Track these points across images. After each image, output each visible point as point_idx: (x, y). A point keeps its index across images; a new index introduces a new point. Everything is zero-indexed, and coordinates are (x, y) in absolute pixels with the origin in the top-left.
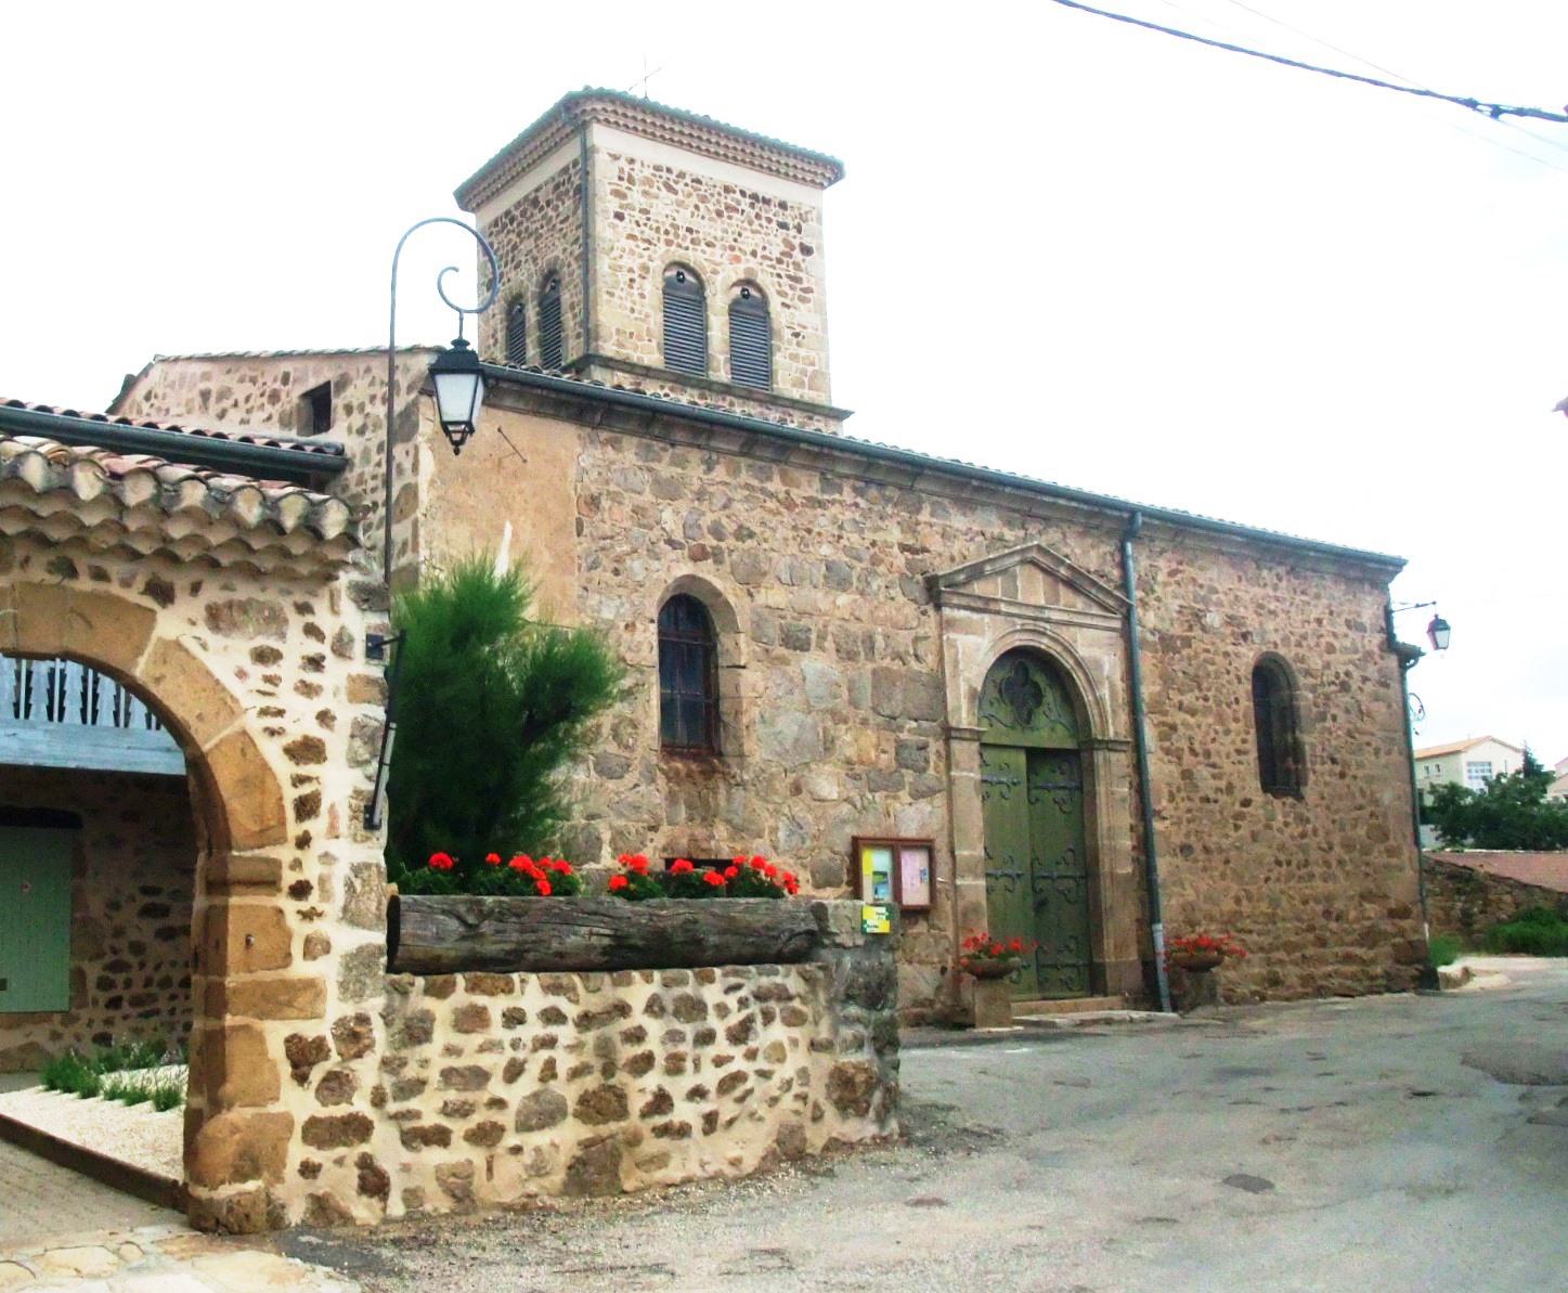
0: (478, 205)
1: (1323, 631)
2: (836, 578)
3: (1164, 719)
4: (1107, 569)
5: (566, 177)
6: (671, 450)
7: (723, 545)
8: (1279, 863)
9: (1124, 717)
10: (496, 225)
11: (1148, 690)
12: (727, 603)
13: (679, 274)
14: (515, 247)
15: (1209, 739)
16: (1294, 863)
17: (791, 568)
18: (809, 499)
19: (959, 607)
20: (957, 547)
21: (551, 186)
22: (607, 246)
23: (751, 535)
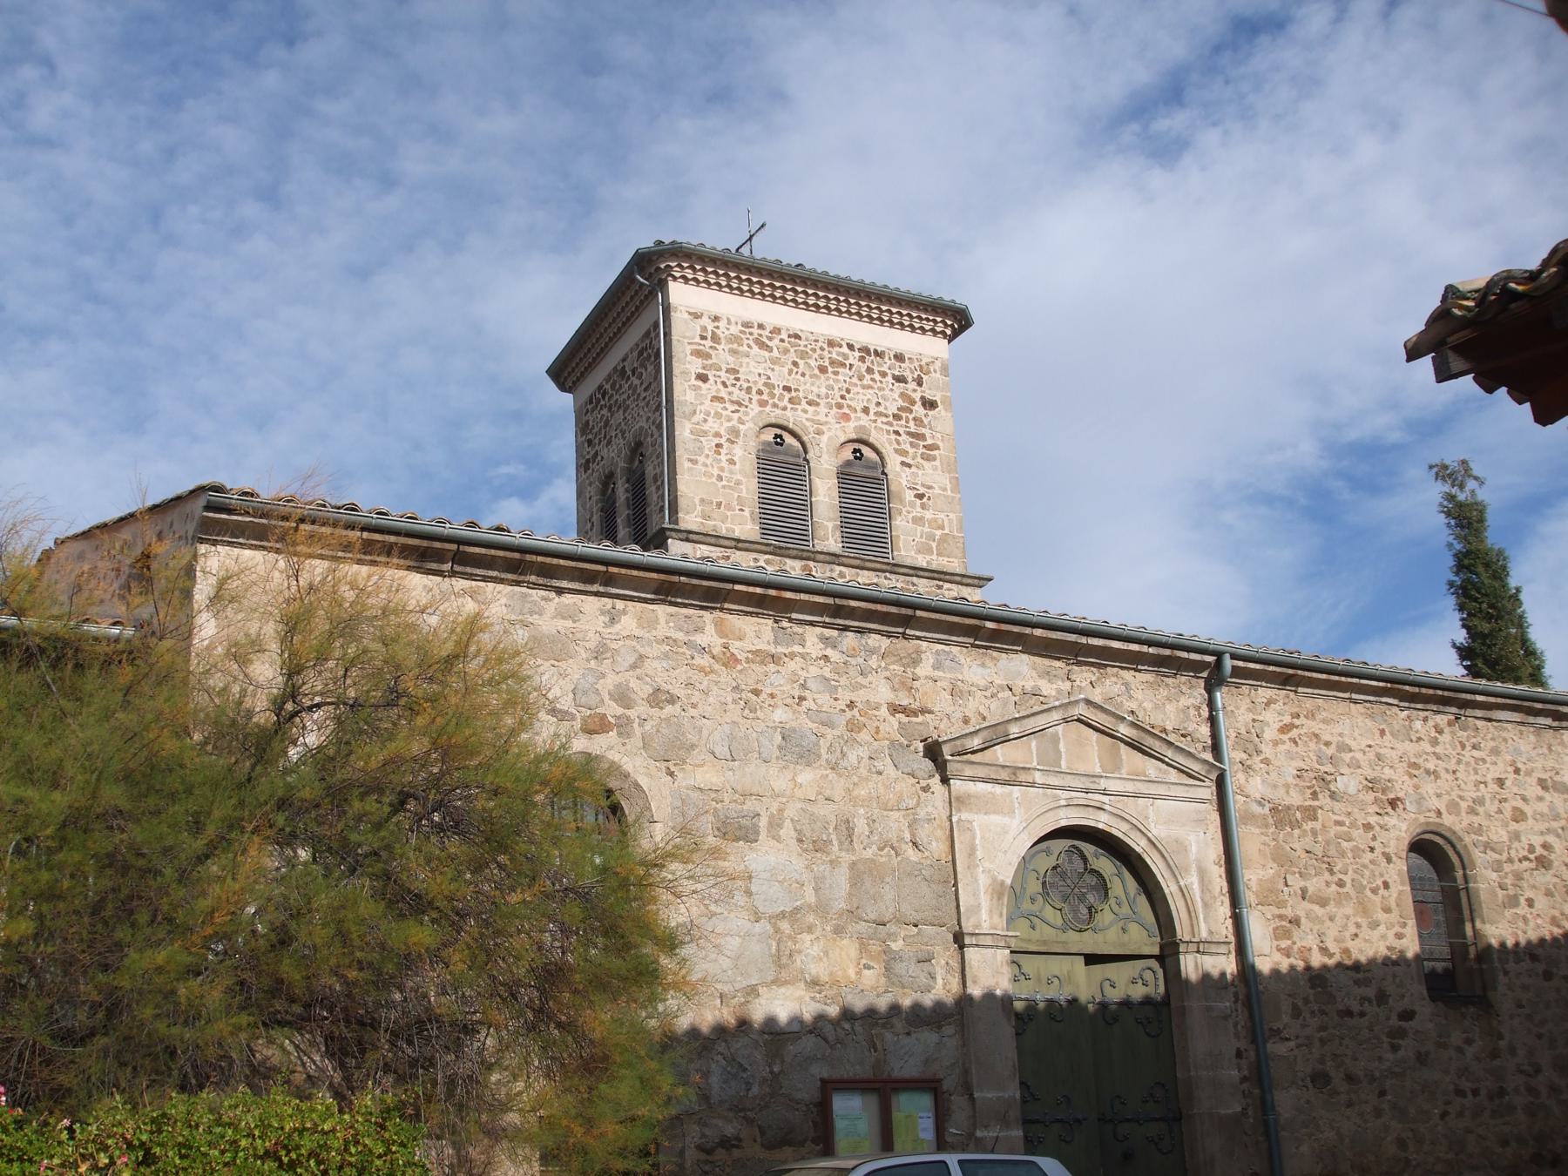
0: (574, 383)
1: (1505, 794)
2: (796, 749)
3: (1282, 911)
4: (1191, 727)
5: (648, 341)
6: (557, 600)
7: (632, 713)
8: (1460, 1093)
9: (1224, 910)
10: (591, 402)
11: (1252, 877)
12: (637, 785)
13: (777, 436)
14: (607, 423)
15: (1347, 934)
16: (1483, 1092)
17: (731, 738)
18: (756, 652)
19: (973, 779)
20: (972, 706)
21: (635, 354)
22: (687, 409)
23: (672, 700)
